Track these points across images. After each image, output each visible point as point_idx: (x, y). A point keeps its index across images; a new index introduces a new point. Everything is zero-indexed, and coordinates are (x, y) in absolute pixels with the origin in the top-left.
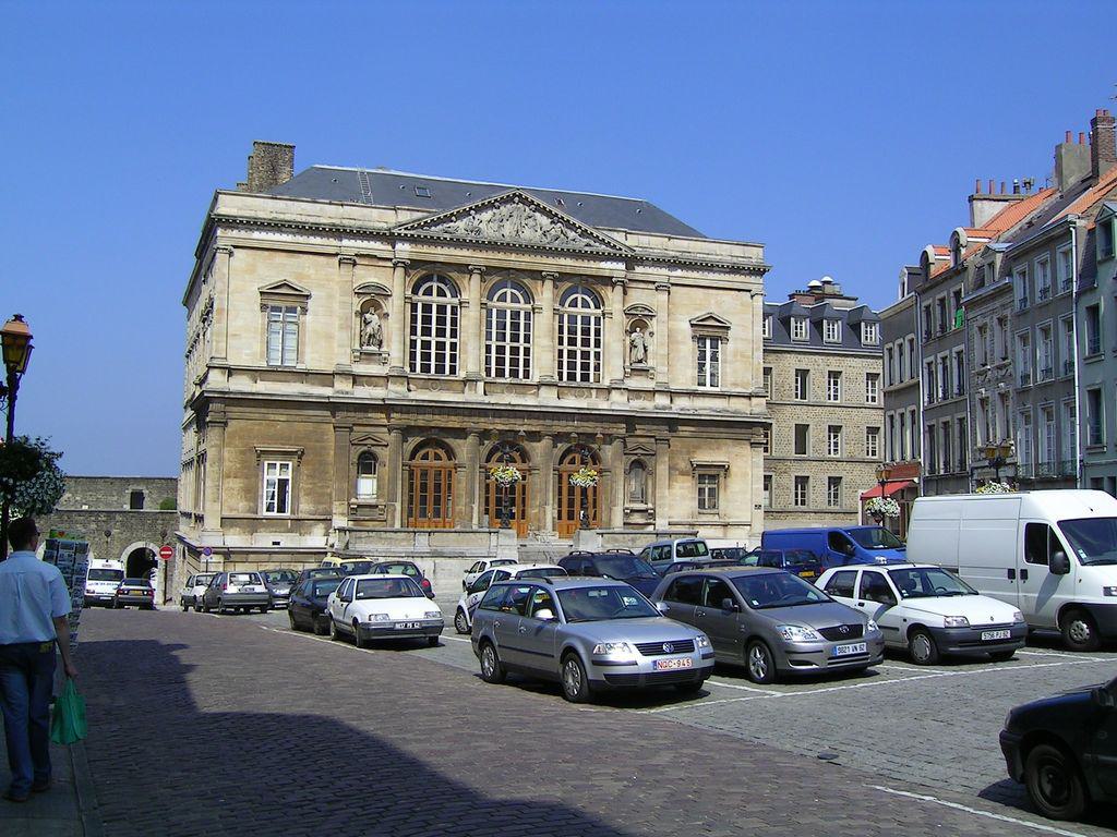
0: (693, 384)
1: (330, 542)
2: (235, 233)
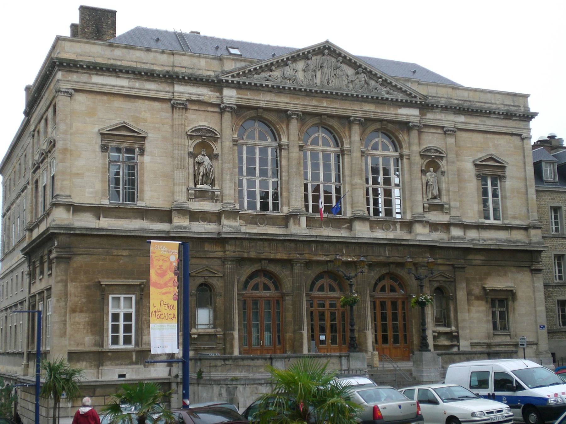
0: (480, 217)
1: (174, 373)
2: (74, 77)
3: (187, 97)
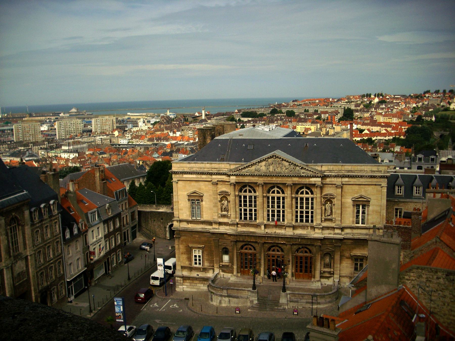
3: (218, 179)
